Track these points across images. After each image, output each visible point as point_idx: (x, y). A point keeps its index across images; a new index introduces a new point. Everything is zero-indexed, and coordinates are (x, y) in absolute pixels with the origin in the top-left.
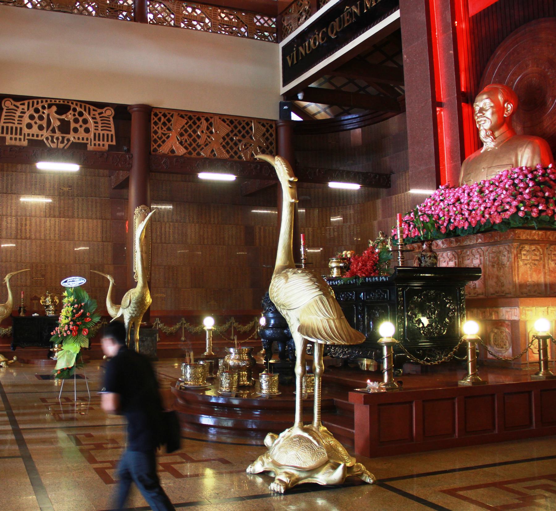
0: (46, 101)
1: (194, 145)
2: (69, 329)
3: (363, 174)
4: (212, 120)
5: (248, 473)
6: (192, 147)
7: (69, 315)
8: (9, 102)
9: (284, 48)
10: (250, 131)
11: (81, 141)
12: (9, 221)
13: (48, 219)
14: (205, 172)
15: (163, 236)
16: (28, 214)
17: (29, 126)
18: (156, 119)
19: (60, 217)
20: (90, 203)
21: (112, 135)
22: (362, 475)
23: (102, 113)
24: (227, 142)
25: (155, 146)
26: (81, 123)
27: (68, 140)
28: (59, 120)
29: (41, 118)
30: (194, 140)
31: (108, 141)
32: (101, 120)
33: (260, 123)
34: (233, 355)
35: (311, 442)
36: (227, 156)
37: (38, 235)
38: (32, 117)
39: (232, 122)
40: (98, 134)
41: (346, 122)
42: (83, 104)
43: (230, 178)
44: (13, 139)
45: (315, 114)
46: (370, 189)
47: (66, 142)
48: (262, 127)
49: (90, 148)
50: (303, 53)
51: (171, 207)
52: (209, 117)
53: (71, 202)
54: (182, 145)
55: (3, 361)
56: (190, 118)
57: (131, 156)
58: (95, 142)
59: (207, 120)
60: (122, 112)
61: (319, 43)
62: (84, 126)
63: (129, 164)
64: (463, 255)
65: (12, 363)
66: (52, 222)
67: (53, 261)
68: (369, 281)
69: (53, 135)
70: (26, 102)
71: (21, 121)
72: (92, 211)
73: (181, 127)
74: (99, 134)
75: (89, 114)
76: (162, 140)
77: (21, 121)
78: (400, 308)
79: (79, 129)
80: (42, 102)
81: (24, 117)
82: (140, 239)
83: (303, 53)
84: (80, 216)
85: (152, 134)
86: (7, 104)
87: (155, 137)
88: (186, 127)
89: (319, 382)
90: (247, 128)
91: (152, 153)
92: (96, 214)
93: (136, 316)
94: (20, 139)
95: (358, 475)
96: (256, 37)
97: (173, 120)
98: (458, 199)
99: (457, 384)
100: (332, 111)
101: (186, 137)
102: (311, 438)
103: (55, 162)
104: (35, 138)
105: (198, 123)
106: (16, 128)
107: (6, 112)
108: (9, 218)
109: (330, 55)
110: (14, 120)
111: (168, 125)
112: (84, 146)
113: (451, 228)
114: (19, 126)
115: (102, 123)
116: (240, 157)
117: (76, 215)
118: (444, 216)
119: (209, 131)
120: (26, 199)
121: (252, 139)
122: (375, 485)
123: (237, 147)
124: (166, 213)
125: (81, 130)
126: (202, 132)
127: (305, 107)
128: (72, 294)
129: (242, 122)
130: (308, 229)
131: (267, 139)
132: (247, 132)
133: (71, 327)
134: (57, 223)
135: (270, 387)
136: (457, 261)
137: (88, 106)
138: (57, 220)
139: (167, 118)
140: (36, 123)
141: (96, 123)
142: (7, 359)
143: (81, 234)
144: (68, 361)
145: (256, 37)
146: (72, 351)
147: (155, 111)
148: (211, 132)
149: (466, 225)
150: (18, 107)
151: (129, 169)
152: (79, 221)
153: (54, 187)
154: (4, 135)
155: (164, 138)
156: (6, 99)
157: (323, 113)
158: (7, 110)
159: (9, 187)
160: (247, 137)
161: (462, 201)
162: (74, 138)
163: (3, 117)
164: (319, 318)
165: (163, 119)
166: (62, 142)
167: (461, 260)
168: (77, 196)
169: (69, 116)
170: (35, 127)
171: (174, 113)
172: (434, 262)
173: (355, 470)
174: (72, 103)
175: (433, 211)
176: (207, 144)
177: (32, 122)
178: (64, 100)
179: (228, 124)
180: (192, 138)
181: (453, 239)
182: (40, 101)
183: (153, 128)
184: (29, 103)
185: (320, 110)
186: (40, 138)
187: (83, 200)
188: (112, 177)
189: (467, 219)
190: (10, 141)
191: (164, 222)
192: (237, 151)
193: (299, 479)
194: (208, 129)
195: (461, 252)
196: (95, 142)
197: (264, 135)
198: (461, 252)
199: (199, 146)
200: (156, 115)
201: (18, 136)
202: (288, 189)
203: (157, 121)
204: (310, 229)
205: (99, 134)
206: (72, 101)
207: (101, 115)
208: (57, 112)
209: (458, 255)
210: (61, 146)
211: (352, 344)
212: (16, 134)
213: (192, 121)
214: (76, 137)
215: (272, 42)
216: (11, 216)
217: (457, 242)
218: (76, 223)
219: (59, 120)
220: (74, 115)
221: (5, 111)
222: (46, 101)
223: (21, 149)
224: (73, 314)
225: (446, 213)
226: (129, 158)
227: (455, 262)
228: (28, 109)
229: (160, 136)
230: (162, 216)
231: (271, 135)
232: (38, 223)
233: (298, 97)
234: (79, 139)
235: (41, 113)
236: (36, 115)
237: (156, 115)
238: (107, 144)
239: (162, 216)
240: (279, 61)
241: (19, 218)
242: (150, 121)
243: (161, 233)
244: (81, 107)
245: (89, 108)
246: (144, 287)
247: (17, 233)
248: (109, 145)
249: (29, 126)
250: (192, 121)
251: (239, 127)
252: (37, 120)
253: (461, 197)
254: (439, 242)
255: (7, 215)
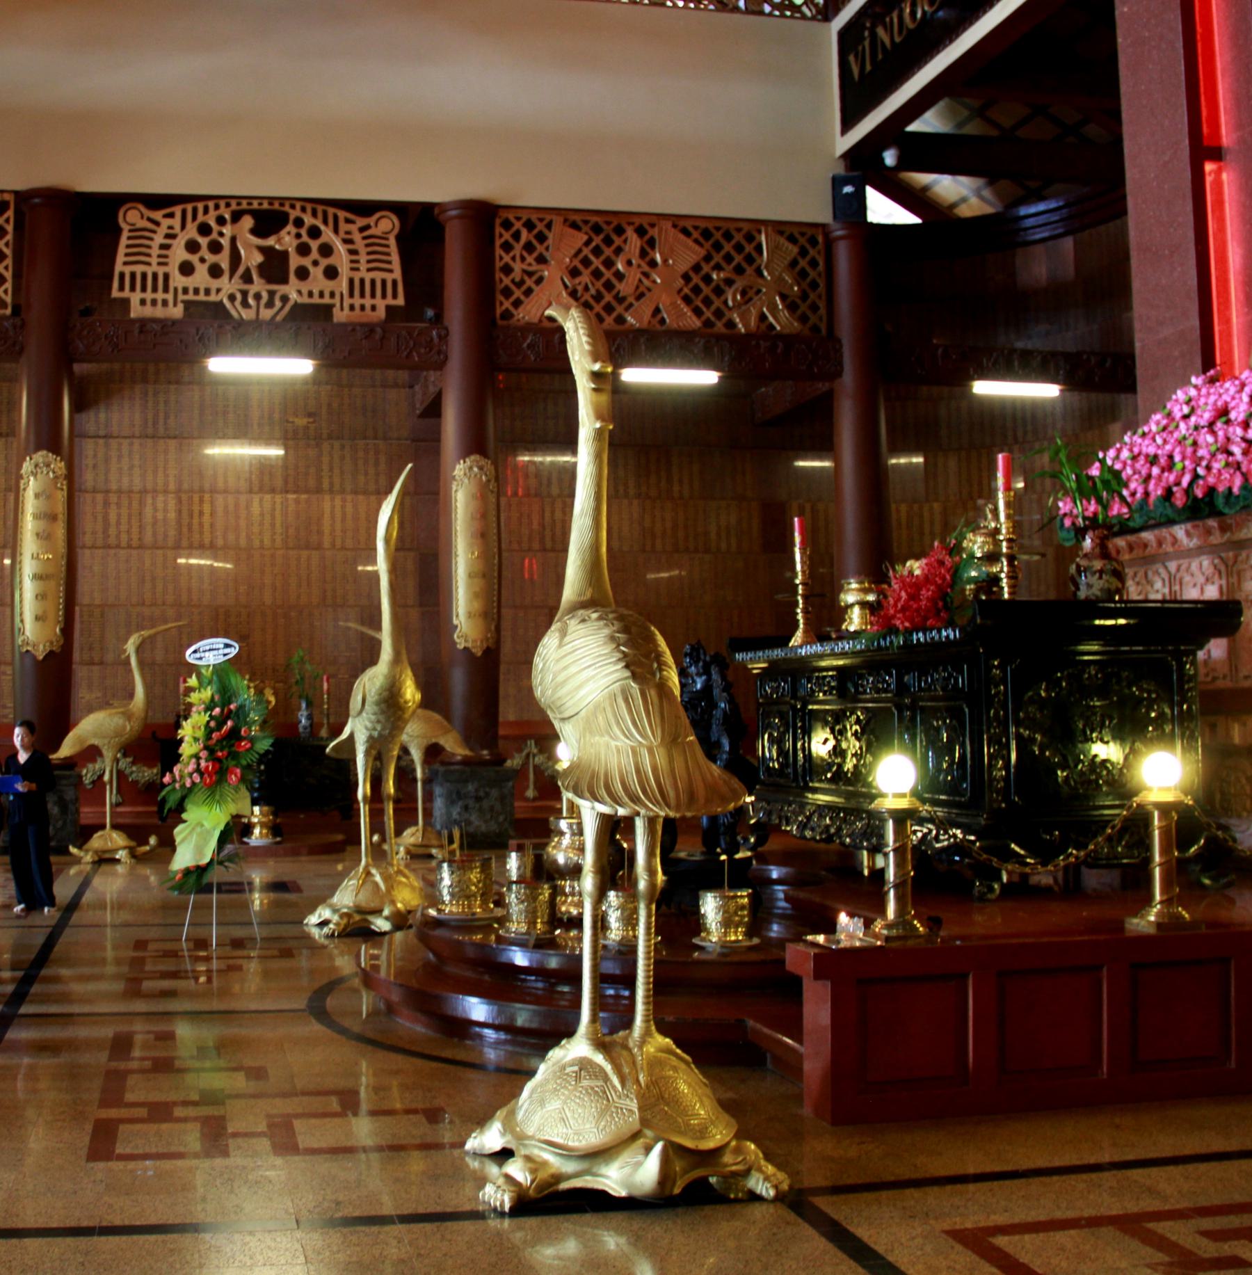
0: (228, 205)
1: (608, 298)
2: (198, 770)
3: (1067, 356)
4: (654, 232)
5: (467, 1153)
6: (603, 303)
7: (200, 734)
8: (391, 226)
9: (843, 34)
10: (754, 254)
11: (316, 300)
12: (160, 505)
13: (256, 498)
14: (637, 366)
15: (548, 533)
16: (207, 486)
17: (187, 269)
18: (507, 236)
19: (287, 492)
20: (361, 454)
21: (395, 283)
22: (747, 1173)
23: (368, 227)
24: (608, 281)
25: (507, 304)
26: (315, 254)
27: (285, 299)
28: (262, 250)
29: (215, 248)
30: (609, 286)
31: (384, 296)
32: (367, 245)
33: (781, 233)
34: (568, 836)
35: (606, 1078)
36: (696, 323)
37: (231, 537)
38: (192, 247)
39: (706, 234)
40: (362, 282)
41: (1029, 222)
42: (320, 208)
43: (707, 378)
44: (149, 302)
45: (953, 206)
46: (1093, 396)
47: (278, 304)
48: (787, 244)
49: (340, 316)
50: (887, 42)
51: (281, 452)
52: (645, 226)
53: (312, 453)
54: (576, 299)
55: (125, 848)
56: (597, 229)
57: (443, 333)
58: (351, 301)
59: (641, 231)
60: (420, 225)
61: (924, 13)
62: (324, 262)
63: (439, 352)
64: (1241, 567)
65: (146, 853)
66: (267, 506)
67: (268, 599)
68: (918, 640)
69: (246, 287)
70: (177, 210)
71: (166, 257)
72: (366, 474)
73: (573, 252)
74: (362, 281)
75: (336, 231)
76: (524, 288)
77: (166, 257)
78: (997, 713)
79: (311, 269)
80: (217, 207)
81: (173, 248)
82: (387, 540)
83: (887, 42)
84: (337, 487)
85: (499, 275)
86: (132, 217)
87: (507, 281)
88: (586, 251)
89: (649, 916)
90: (749, 248)
91: (500, 322)
92: (377, 481)
93: (380, 735)
94: (165, 303)
95: (735, 1174)
96: (767, 8)
97: (550, 236)
98: (1223, 412)
99: (1120, 927)
100: (999, 195)
101: (586, 278)
102: (608, 1068)
103: (251, 355)
104: (202, 297)
105: (618, 241)
106: (155, 276)
107: (129, 238)
108: (161, 498)
109: (951, 41)
110: (149, 255)
111: (540, 248)
112: (325, 312)
113: (1199, 493)
114: (161, 271)
115: (369, 253)
116: (731, 324)
117: (326, 485)
118: (1183, 459)
119: (647, 259)
120: (220, 451)
121: (762, 276)
122: (778, 1204)
123: (723, 298)
124: (554, 476)
125: (317, 273)
126: (629, 263)
127: (926, 189)
128: (210, 682)
129: (734, 233)
130: (931, 509)
131: (803, 274)
132: (750, 260)
133: (203, 764)
134: (278, 507)
135: (727, 923)
136: (1224, 582)
137: (331, 211)
138: (278, 498)
139: (535, 231)
140: (202, 260)
141: (353, 252)
142: (133, 844)
143: (338, 533)
144: (199, 850)
145: (767, 8)
146: (207, 825)
147: (504, 214)
148: (653, 264)
149: (1238, 481)
150: (157, 224)
151: (441, 366)
152: (332, 500)
153: (270, 418)
154: (127, 293)
155: (529, 282)
156: (128, 206)
157: (974, 200)
158: (130, 231)
159: (161, 421)
160: (750, 271)
161: (1233, 415)
162: (299, 292)
163: (122, 250)
164: (613, 743)
165: (525, 235)
166: (270, 304)
167: (1234, 580)
168: (330, 437)
169: (286, 240)
170: (201, 272)
171: (554, 218)
172: (1113, 587)
173: (728, 1158)
174: (293, 207)
175: (1158, 447)
176: (641, 295)
177: (194, 259)
178: (271, 200)
179: (696, 241)
180: (603, 280)
181: (1212, 523)
182: (211, 204)
183: (501, 258)
184: (184, 213)
185: (964, 192)
186: (213, 298)
187: (343, 447)
188: (417, 388)
189: (1238, 466)
190: (139, 308)
191: (549, 495)
192: (722, 307)
193: (558, 1178)
194: (643, 254)
195: (1236, 557)
196: (351, 301)
197: (794, 263)
198: (1236, 557)
199: (620, 300)
200: (507, 225)
201: (160, 296)
202: (588, 393)
203: (511, 240)
204: (936, 505)
205: (362, 281)
206: (292, 201)
207: (366, 233)
208: (255, 232)
209: (1227, 566)
210: (266, 314)
211: (689, 814)
212: (155, 290)
213: (601, 236)
214: (305, 292)
215: (813, 18)
216: (166, 492)
217: (1224, 529)
218: (327, 505)
219: (262, 250)
220: (298, 236)
221: (125, 234)
222: (228, 205)
223: (166, 326)
224: (209, 731)
225: (1189, 450)
226: (440, 337)
227: (1221, 587)
228: (183, 227)
229: (517, 280)
230: (545, 482)
231: (813, 263)
232: (231, 508)
233: (882, 160)
234: (310, 294)
235: (214, 235)
236: (203, 241)
237: (507, 225)
238: (381, 304)
239: (545, 482)
240: (831, 70)
241: (184, 497)
242: (492, 242)
243: (543, 526)
244: (314, 214)
245: (336, 218)
246: (396, 661)
247: (180, 533)
248: (388, 308)
249: (187, 269)
250: (601, 236)
251: (728, 247)
252: (204, 252)
253: (1232, 404)
254: (1179, 531)
255: (155, 491)
